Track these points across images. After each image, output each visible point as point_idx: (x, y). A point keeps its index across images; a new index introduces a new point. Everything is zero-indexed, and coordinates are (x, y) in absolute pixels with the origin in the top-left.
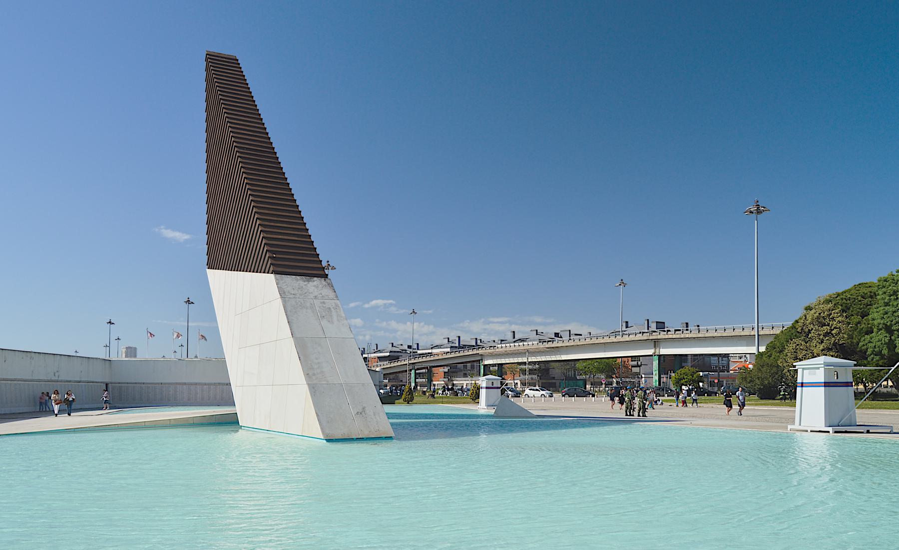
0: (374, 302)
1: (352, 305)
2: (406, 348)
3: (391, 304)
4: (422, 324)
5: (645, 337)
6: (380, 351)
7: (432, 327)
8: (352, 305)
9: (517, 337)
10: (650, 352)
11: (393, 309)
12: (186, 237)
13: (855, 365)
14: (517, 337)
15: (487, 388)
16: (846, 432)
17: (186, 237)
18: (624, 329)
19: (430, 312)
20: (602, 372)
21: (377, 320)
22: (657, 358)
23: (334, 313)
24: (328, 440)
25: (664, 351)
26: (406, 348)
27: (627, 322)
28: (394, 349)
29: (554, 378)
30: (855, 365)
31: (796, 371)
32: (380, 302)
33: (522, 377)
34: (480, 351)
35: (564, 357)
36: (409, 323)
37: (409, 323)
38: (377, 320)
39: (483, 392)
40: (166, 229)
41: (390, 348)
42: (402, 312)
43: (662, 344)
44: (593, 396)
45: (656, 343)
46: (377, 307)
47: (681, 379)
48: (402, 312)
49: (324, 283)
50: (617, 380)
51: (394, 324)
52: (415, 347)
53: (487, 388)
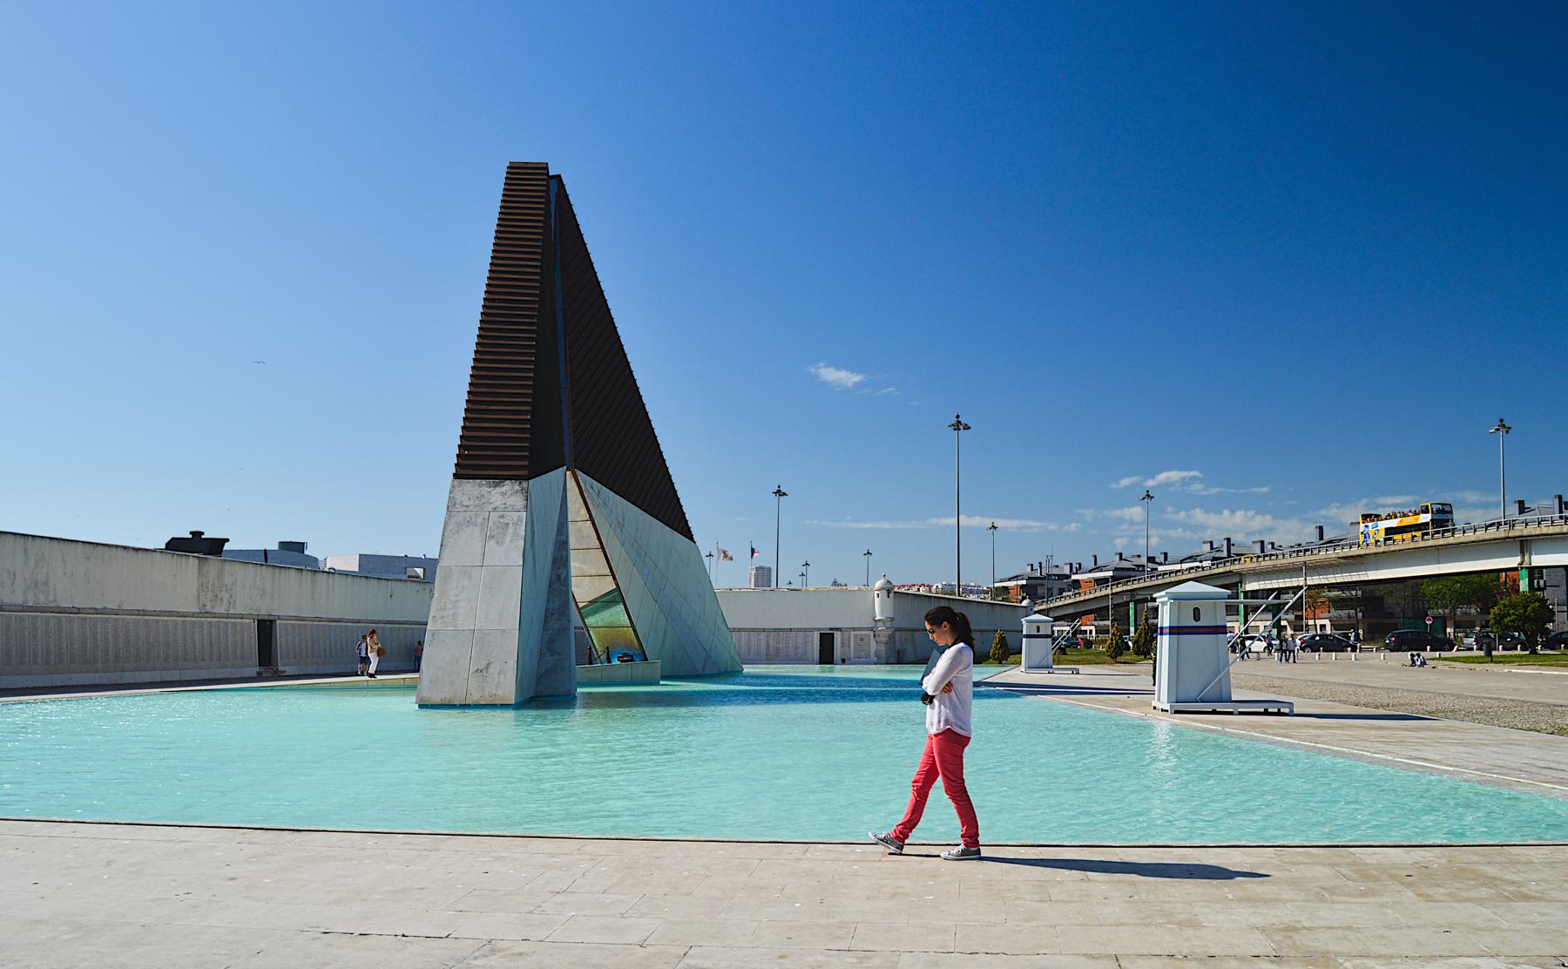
0: (1163, 477)
1: (1125, 482)
2: (1144, 560)
3: (1194, 479)
4: (1250, 513)
5: (1501, 533)
6: (1098, 569)
7: (1268, 517)
8: (1125, 482)
9: (1326, 538)
10: (1513, 562)
11: (1197, 486)
12: (857, 378)
13: (1229, 597)
14: (1326, 538)
15: (1175, 630)
16: (1214, 712)
17: (857, 378)
18: (1516, 516)
19: (1264, 490)
20: (1469, 602)
21: (1170, 509)
22: (1524, 573)
23: (510, 531)
24: (421, 706)
25: (1538, 560)
26: (1144, 560)
27: (1521, 503)
28: (1124, 564)
29: (1392, 615)
30: (1229, 597)
31: (1156, 609)
32: (1174, 475)
33: (1334, 613)
34: (1236, 567)
35: (1373, 575)
36: (1226, 512)
37: (1226, 512)
38: (1170, 509)
39: (1164, 643)
40: (826, 366)
41: (1116, 562)
42: (1213, 491)
43: (1534, 546)
44: (1354, 650)
45: (1524, 545)
46: (1167, 484)
47: (1505, 616)
48: (1213, 491)
49: (517, 487)
50: (1395, 617)
51: (1199, 515)
52: (1161, 559)
53: (1175, 630)
